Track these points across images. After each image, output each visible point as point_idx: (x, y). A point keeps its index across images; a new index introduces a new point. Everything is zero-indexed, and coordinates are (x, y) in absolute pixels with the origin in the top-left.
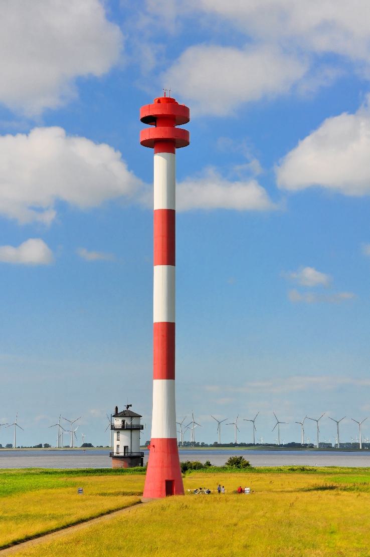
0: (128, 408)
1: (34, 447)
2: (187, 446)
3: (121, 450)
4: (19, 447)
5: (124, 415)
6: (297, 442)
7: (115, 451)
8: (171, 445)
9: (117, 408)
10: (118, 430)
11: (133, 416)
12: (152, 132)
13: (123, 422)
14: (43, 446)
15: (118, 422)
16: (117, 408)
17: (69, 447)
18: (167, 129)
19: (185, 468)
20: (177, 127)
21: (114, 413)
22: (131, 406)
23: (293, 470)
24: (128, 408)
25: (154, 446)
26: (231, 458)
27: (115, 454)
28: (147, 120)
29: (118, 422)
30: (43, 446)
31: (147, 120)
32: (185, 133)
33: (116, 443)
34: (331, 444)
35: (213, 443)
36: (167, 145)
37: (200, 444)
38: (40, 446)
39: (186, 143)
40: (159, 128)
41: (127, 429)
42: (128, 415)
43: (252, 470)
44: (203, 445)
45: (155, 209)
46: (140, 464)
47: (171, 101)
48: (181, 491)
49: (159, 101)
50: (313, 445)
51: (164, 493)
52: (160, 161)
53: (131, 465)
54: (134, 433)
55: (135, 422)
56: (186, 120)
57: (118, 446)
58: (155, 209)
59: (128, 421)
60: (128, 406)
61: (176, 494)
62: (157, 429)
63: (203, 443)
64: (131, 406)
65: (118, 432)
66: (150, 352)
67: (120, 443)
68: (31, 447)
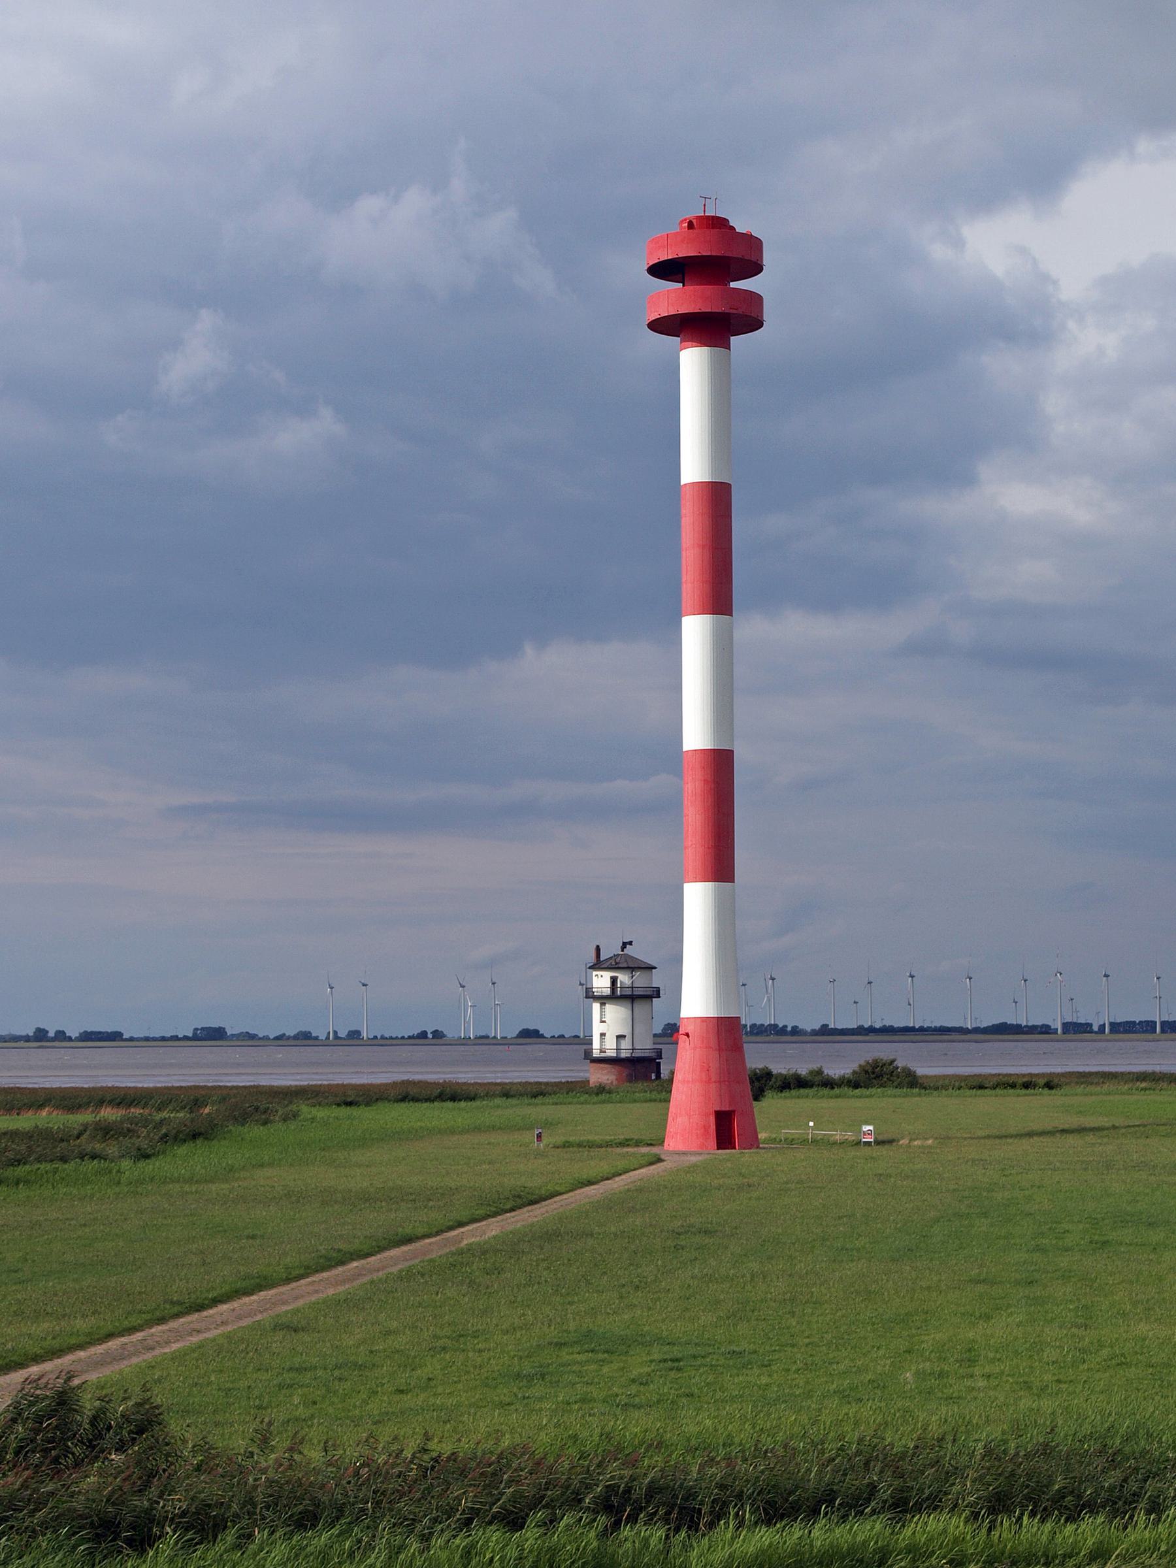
0: (623, 948)
1: (409, 1037)
2: (757, 1034)
3: (611, 1044)
4: (376, 1037)
5: (614, 965)
6: (1011, 1021)
7: (596, 1044)
8: (727, 1032)
9: (598, 949)
10: (603, 1000)
11: (634, 966)
12: (672, 297)
13: (614, 981)
14: (430, 1036)
15: (601, 981)
16: (598, 949)
17: (487, 1037)
18: (709, 290)
19: (762, 1083)
20: (733, 285)
21: (592, 959)
22: (630, 943)
23: (1049, 1086)
24: (623, 948)
25: (687, 1035)
26: (893, 1061)
27: (596, 1053)
28: (660, 270)
29: (601, 981)
30: (430, 1036)
31: (660, 270)
32: (755, 299)
33: (597, 1028)
34: (1091, 1025)
35: (817, 1027)
36: (714, 327)
37: (789, 1029)
38: (423, 1035)
39: (755, 324)
40: (690, 289)
41: (623, 997)
42: (625, 965)
43: (911, 1081)
44: (795, 1031)
45: (685, 748)
46: (653, 1077)
47: (718, 224)
48: (753, 1142)
49: (691, 225)
50: (1049, 1026)
51: (712, 1142)
52: (693, 362)
53: (633, 1078)
54: (640, 1007)
55: (641, 980)
56: (755, 268)
57: (603, 1035)
58: (685, 748)
59: (624, 978)
60: (624, 945)
61: (741, 1147)
62: (697, 998)
63: (795, 1028)
64: (630, 943)
65: (603, 1004)
66: (693, 817)
67: (608, 1028)
68: (403, 1038)
